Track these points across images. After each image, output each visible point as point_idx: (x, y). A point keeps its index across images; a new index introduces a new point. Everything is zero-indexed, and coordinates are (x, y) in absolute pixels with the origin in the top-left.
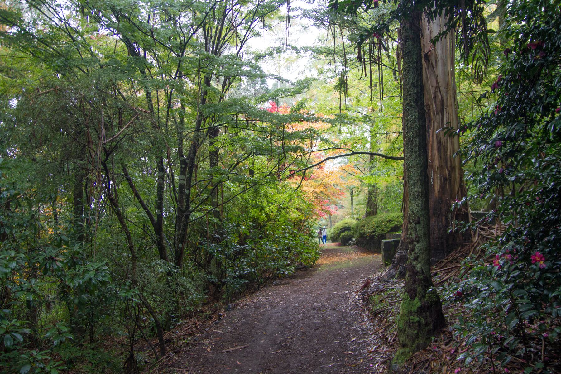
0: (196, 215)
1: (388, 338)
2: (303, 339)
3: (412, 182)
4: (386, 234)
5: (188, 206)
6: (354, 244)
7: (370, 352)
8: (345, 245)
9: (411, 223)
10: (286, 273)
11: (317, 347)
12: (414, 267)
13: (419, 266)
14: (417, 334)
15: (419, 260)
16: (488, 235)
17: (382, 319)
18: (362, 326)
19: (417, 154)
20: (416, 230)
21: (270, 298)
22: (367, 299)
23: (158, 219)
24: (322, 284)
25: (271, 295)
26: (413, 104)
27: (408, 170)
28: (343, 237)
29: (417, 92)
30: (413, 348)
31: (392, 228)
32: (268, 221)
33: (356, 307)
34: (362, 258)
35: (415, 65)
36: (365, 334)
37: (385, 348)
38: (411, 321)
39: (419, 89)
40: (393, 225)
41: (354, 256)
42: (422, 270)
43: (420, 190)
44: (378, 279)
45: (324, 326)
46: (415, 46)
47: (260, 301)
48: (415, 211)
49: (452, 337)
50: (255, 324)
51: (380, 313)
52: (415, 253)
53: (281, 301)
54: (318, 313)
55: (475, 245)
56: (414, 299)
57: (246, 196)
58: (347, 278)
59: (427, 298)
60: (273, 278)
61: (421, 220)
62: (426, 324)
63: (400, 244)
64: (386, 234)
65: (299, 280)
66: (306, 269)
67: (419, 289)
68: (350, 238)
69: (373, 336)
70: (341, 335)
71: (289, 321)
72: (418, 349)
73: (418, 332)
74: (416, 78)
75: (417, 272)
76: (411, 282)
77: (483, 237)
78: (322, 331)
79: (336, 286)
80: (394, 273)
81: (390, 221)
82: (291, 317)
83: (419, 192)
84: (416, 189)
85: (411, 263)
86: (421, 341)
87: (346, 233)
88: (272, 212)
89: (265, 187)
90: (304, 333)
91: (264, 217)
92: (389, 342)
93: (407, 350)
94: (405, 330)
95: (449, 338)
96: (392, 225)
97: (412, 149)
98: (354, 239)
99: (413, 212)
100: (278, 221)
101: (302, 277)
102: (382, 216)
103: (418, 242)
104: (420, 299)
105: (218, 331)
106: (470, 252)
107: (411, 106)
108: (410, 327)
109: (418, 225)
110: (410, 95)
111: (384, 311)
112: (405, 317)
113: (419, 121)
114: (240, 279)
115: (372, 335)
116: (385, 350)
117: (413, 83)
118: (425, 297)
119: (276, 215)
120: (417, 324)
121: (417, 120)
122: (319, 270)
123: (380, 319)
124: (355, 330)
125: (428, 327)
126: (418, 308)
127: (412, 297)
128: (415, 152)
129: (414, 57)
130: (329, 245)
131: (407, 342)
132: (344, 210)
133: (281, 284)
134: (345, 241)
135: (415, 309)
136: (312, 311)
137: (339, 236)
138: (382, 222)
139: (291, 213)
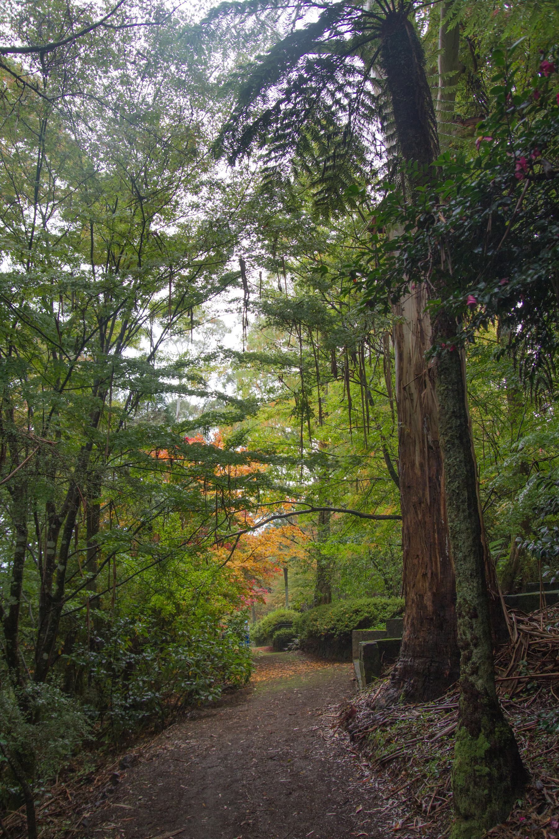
0: (71, 605)
1: (421, 804)
2: (272, 813)
3: (461, 555)
4: (351, 631)
5: (61, 590)
6: (297, 649)
7: (396, 831)
8: (281, 650)
9: (464, 617)
10: (210, 698)
11: (302, 826)
12: (473, 685)
13: (480, 684)
14: (489, 795)
15: (480, 673)
16: (532, 630)
17: (396, 772)
18: (364, 784)
19: (466, 513)
20: (471, 628)
21: (193, 742)
22: (360, 739)
23: (11, 614)
24: (269, 716)
25: (191, 737)
26: (456, 441)
27: (454, 537)
28: (278, 639)
29: (461, 425)
30: (484, 820)
31: (360, 622)
32: (178, 614)
33: (342, 752)
34: (317, 670)
35: (455, 387)
36: (375, 798)
37: (420, 823)
38: (477, 774)
39: (463, 420)
40: (362, 618)
41: (302, 667)
42: (485, 689)
43: (474, 567)
44: (368, 705)
45: (300, 787)
46: (454, 360)
47: (178, 747)
48: (468, 598)
49: (544, 799)
50: (182, 788)
51: (390, 761)
52: (473, 663)
53: (213, 746)
54: (282, 766)
55: (517, 646)
56: (478, 737)
57: (146, 575)
58: (305, 704)
59: (498, 733)
60: (188, 707)
61: (478, 612)
62: (501, 778)
63: (402, 648)
64: (351, 631)
65: (229, 710)
66: (236, 692)
67: (485, 720)
68: (289, 638)
69: (390, 801)
70: (334, 803)
71: (237, 781)
72: (492, 822)
73: (490, 791)
74: (457, 405)
75: (479, 693)
76: (470, 710)
77: (526, 634)
78: (300, 797)
79: (293, 717)
80: (396, 695)
81: (357, 612)
82: (239, 774)
83: (473, 570)
84: (468, 565)
85: (466, 680)
86: (495, 807)
87: (283, 631)
88: (184, 600)
89: (176, 562)
90: (270, 802)
91: (170, 608)
92: (425, 812)
93: (475, 823)
94: (468, 790)
95: (539, 800)
96: (360, 618)
97: (458, 507)
98: (297, 641)
99: (464, 599)
100: (194, 614)
101: (231, 704)
102: (339, 606)
103: (476, 645)
104: (487, 736)
105: (122, 805)
106: (511, 658)
107: (453, 444)
108: (476, 784)
109: (474, 620)
110: (451, 428)
111: (397, 758)
112: (466, 768)
113: (466, 466)
114: (136, 710)
115: (387, 799)
116: (420, 825)
117: (454, 412)
118: (494, 733)
119: (190, 605)
120: (487, 778)
121: (463, 464)
122: (255, 692)
123: (393, 772)
124: (355, 792)
125: (505, 784)
126: (486, 751)
127: (475, 734)
128: (464, 511)
129: (453, 375)
130: (260, 651)
131: (472, 810)
132: (274, 594)
133: (201, 718)
134: (281, 644)
135: (481, 753)
136: (271, 763)
137: (271, 636)
138: (345, 613)
139: (213, 602)
